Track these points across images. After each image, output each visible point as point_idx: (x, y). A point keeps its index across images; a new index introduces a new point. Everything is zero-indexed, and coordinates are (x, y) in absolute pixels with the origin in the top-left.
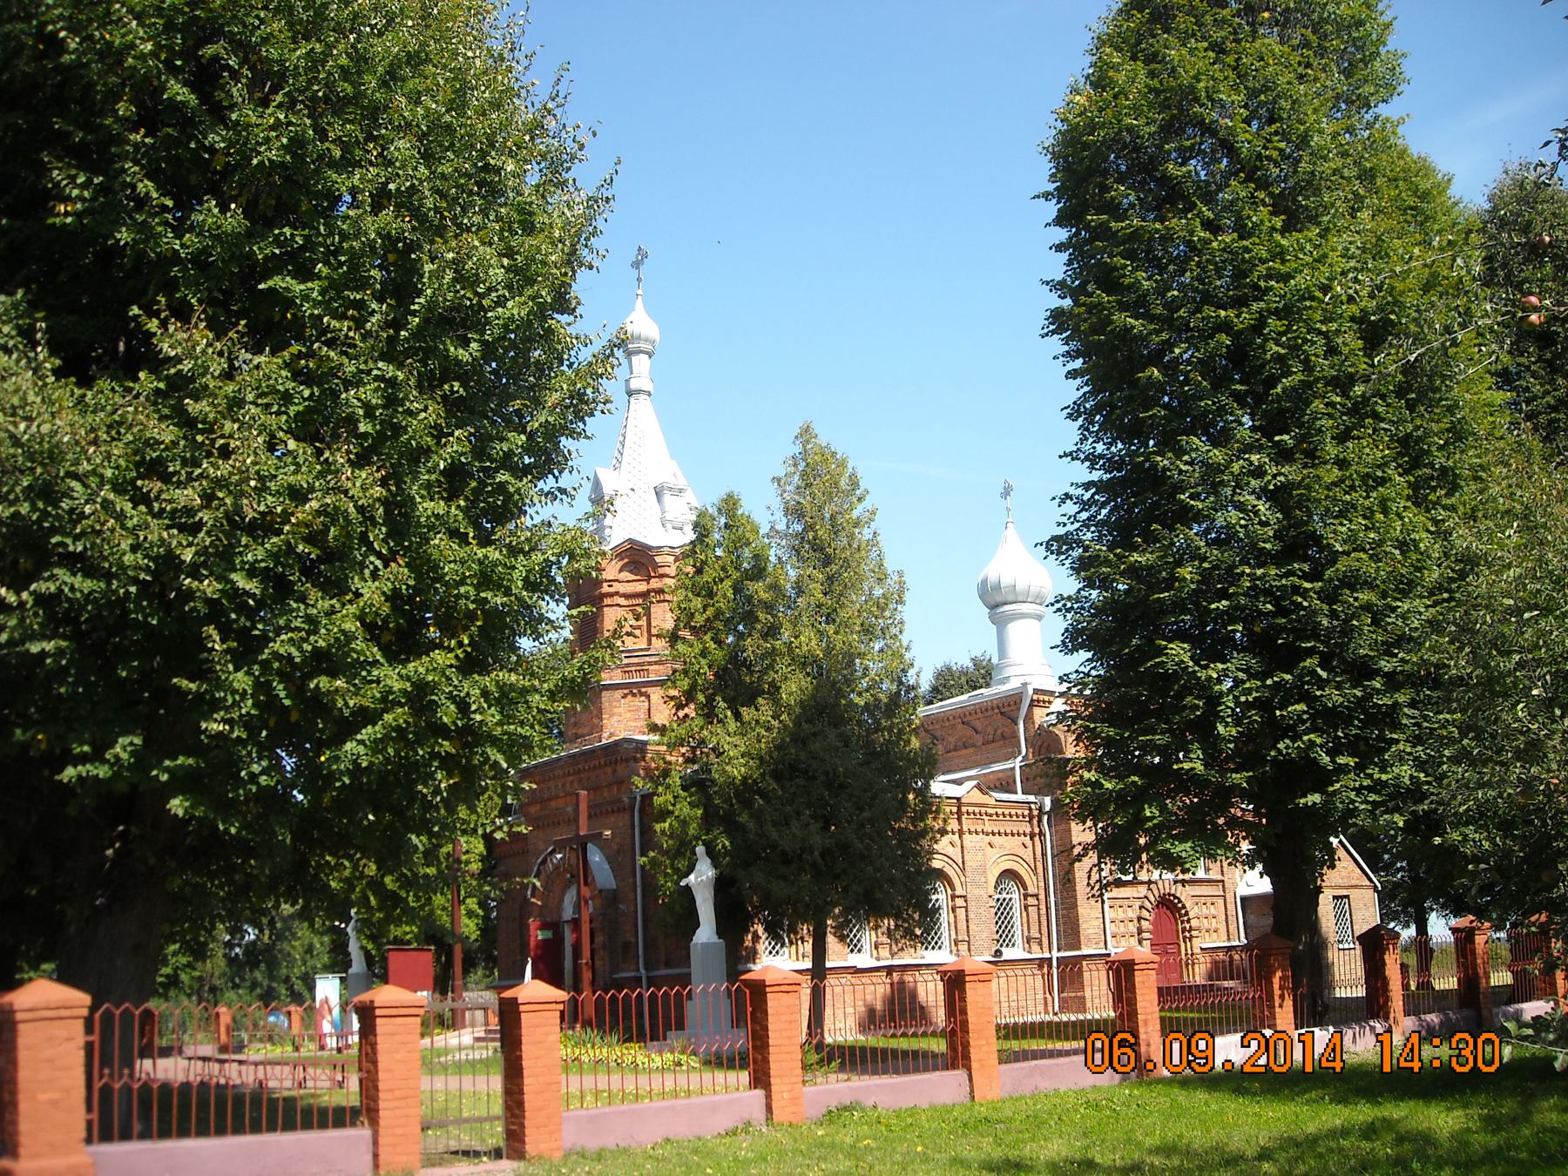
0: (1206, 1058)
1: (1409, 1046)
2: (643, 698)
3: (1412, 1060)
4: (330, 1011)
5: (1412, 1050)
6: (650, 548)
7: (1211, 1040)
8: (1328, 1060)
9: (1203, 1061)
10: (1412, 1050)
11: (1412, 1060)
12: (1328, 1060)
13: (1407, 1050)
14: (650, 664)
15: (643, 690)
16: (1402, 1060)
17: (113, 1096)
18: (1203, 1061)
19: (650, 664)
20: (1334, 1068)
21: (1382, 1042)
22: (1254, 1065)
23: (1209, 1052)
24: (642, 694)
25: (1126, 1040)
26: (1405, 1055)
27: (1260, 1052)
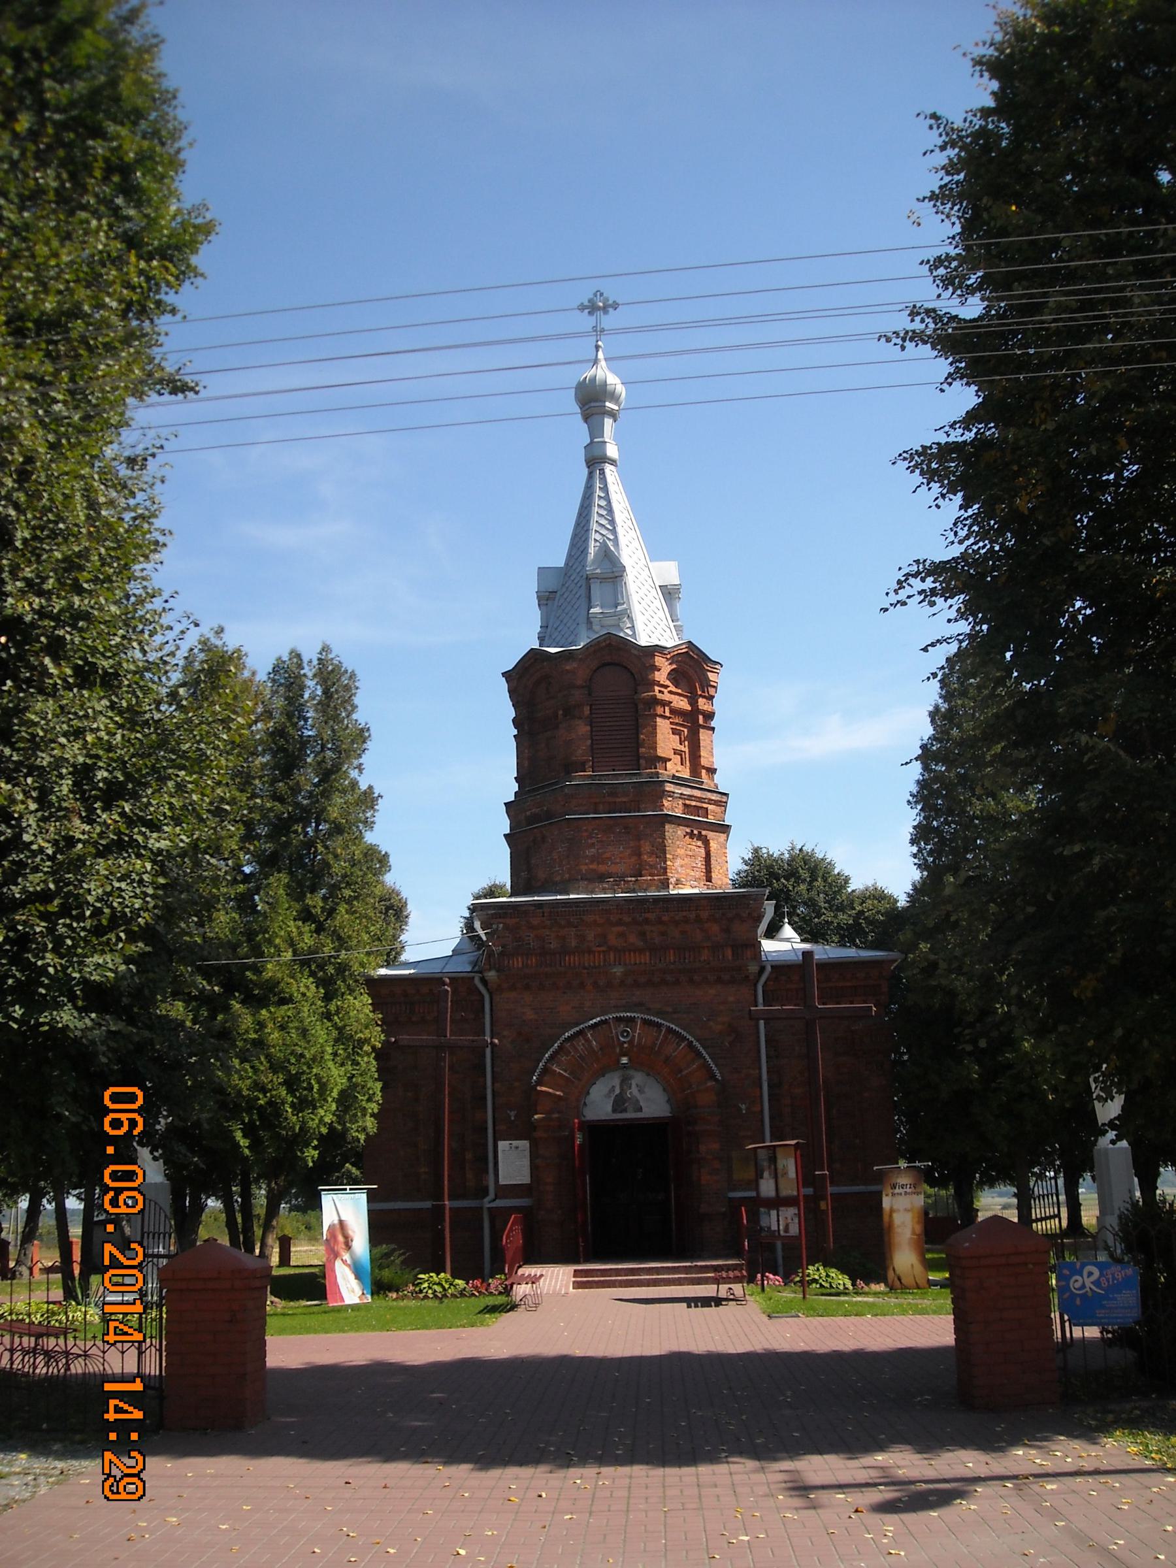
0: (118, 1493)
1: (131, 1331)
2: (699, 843)
3: (116, 1334)
4: (348, 1246)
5: (126, 1334)
6: (707, 659)
7: (135, 1497)
8: (116, 1328)
9: (115, 1489)
10: (126, 1334)
11: (116, 1334)
12: (116, 1328)
13: (126, 1329)
14: (710, 802)
15: (704, 833)
16: (117, 1324)
17: (444, 1213)
18: (115, 1489)
19: (710, 802)
20: (107, 1412)
21: (134, 1303)
22: (111, 1462)
23: (123, 1496)
24: (700, 837)
25: (111, 1201)
26: (121, 1326)
27: (123, 1468)
